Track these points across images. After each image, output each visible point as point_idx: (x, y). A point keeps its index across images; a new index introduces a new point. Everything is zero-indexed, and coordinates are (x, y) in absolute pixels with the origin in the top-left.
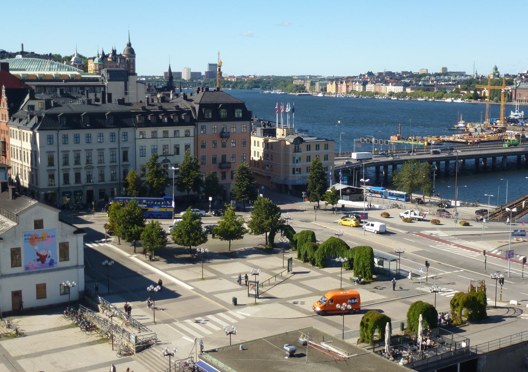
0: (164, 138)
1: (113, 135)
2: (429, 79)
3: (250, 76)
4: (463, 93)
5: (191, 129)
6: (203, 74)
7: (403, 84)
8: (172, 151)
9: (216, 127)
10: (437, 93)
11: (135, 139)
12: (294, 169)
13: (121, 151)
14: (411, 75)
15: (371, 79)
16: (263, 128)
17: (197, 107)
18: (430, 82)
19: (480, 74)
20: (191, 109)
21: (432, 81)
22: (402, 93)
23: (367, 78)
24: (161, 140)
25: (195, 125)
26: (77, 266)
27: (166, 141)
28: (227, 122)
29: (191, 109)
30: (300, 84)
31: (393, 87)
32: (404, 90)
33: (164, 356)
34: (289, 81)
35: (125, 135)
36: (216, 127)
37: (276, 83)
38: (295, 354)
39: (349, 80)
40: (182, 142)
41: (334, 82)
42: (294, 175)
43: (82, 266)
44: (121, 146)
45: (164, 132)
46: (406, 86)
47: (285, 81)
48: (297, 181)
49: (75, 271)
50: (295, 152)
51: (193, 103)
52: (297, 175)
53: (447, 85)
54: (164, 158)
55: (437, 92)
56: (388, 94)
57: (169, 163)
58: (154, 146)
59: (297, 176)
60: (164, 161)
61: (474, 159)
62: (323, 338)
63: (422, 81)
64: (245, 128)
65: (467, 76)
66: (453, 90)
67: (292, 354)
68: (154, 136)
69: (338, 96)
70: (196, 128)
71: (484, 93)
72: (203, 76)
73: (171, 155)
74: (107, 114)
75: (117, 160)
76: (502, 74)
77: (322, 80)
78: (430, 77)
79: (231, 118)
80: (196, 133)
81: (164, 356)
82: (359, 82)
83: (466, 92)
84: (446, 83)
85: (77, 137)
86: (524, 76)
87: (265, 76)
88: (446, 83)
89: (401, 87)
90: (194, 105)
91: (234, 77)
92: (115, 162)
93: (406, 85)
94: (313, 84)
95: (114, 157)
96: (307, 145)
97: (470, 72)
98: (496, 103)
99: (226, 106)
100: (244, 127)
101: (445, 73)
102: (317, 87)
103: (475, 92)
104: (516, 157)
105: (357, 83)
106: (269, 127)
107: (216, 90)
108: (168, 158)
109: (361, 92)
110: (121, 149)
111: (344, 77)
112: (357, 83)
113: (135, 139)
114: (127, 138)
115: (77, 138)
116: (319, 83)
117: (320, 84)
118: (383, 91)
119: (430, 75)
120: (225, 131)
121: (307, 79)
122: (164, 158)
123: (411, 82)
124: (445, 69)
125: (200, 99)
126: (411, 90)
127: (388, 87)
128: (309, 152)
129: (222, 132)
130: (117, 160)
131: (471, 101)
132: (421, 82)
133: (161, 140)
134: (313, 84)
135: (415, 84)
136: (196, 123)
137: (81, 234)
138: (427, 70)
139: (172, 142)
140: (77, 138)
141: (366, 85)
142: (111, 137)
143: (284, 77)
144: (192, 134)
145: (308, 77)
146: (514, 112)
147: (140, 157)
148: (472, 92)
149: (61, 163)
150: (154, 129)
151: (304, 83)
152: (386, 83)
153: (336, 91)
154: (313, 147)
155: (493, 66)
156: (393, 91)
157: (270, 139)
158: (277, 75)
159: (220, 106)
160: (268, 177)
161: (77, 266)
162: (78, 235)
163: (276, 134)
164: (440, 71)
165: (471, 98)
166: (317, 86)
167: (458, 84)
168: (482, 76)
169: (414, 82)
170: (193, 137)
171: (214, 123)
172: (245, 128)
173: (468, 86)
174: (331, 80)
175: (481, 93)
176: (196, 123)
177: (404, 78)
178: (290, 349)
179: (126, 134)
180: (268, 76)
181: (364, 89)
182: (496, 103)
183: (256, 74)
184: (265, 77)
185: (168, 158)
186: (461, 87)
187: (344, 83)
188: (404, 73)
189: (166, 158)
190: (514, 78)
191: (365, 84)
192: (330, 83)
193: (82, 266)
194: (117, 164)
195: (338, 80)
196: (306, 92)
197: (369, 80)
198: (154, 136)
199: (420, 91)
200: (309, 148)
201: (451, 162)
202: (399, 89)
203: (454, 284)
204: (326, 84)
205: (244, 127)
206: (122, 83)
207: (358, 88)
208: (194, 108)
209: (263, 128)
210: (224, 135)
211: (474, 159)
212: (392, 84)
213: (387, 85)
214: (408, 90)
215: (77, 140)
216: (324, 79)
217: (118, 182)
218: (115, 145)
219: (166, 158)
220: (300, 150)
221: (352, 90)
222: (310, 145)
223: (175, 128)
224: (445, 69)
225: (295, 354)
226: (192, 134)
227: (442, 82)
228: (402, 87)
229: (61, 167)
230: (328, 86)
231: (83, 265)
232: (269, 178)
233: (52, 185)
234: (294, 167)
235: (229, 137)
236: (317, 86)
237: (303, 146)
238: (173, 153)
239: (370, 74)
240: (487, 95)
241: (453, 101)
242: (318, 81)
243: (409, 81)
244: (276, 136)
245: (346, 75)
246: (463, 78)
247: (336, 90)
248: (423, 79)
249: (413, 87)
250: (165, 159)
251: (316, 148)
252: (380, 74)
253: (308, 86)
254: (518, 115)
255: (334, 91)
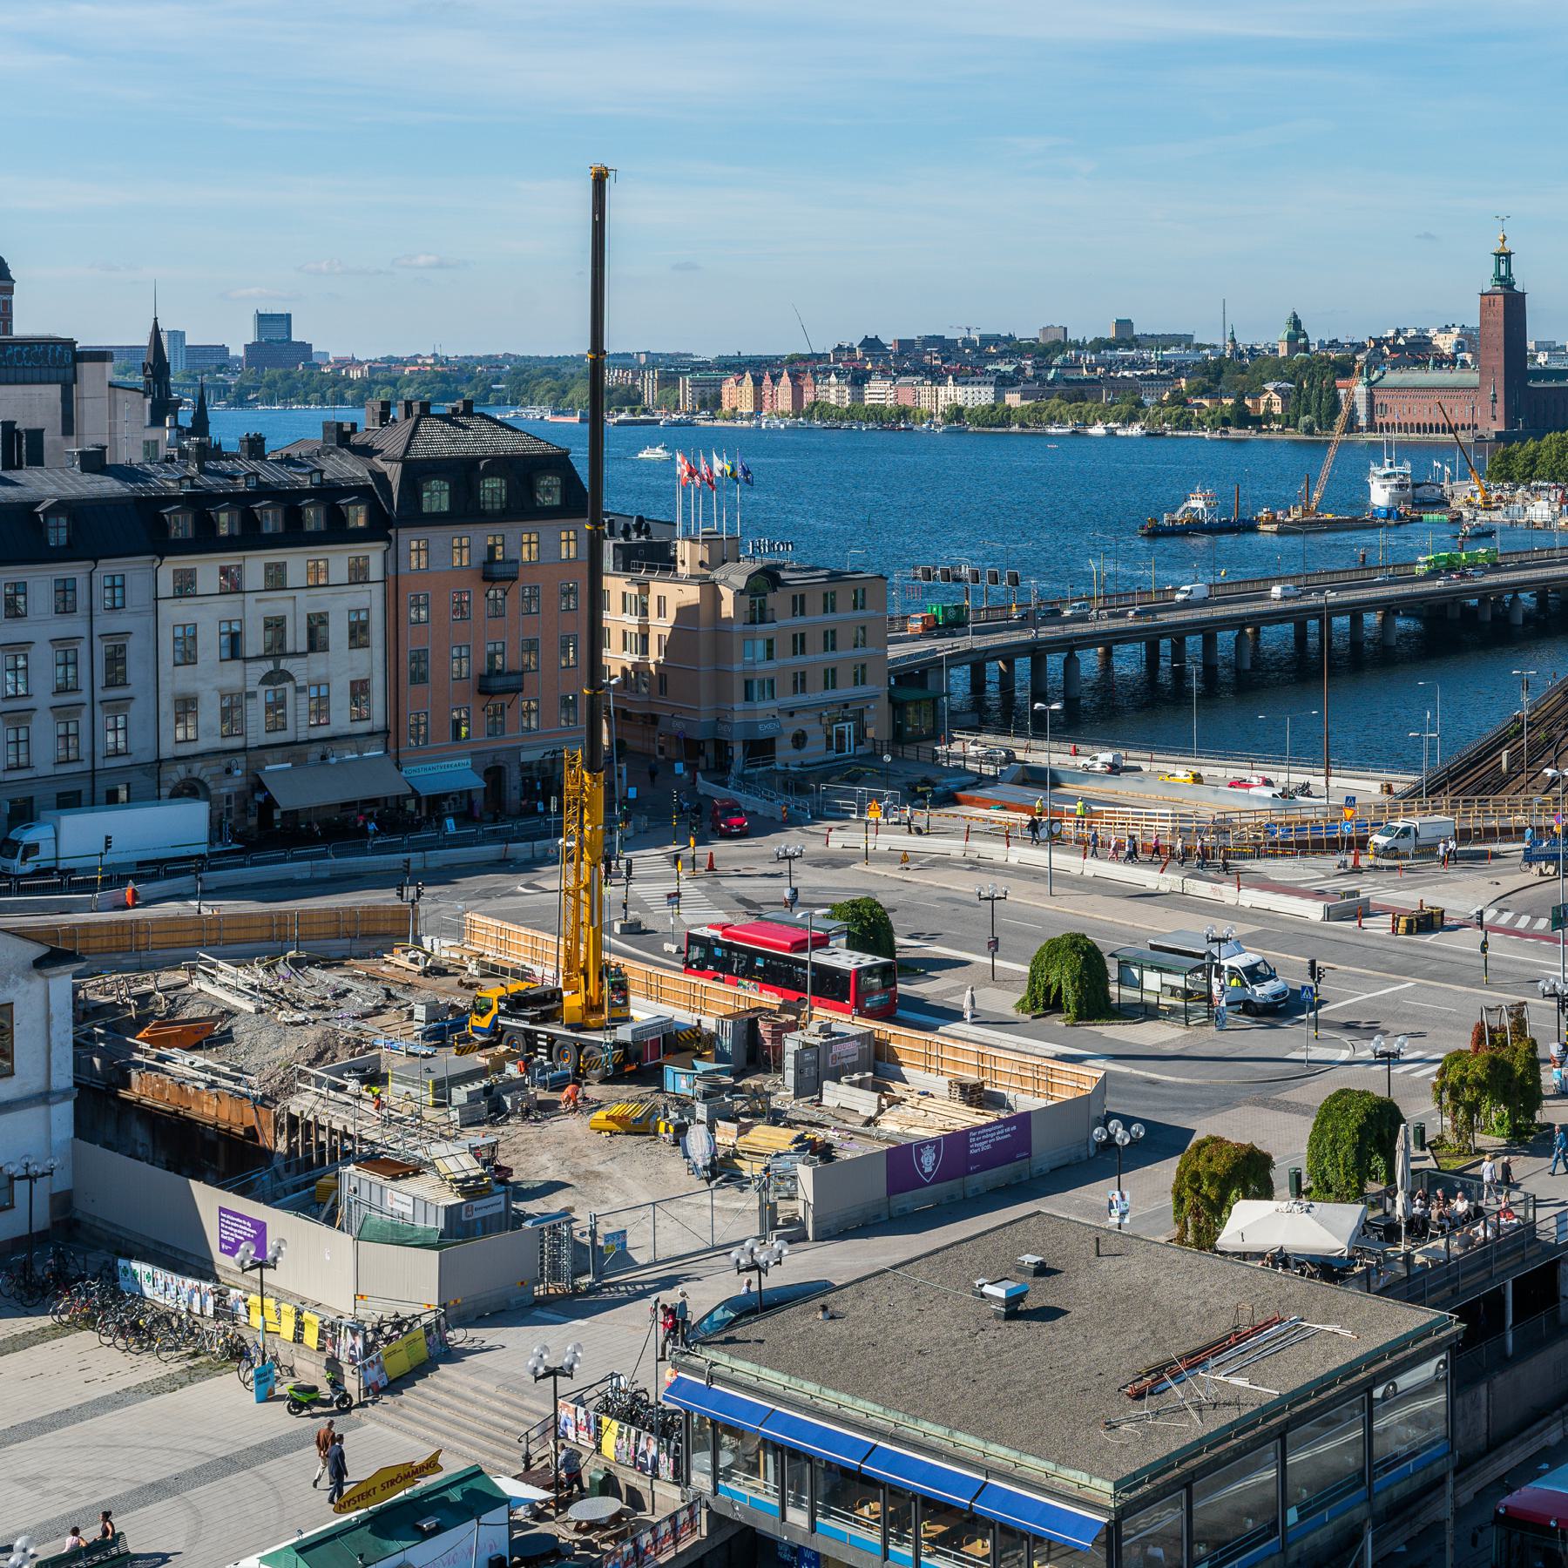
0: (351, 583)
1: (65, 590)
2: (1077, 358)
3: (419, 356)
4: (1200, 406)
5: (374, 554)
6: (237, 351)
7: (993, 379)
8: (296, 637)
9: (465, 542)
10: (1113, 408)
11: (156, 599)
12: (748, 684)
13: (100, 648)
14: (1011, 347)
15: (875, 363)
16: (622, 540)
17: (394, 472)
18: (1085, 372)
19: (1244, 341)
20: (371, 482)
21: (1092, 368)
22: (994, 408)
23: (862, 360)
24: (258, 601)
25: (388, 539)
26: (45, 1097)
27: (278, 604)
28: (471, 527)
29: (371, 482)
30: (622, 385)
31: (960, 390)
32: (999, 397)
33: (537, 1379)
34: (572, 376)
35: (118, 585)
36: (465, 542)
37: (527, 382)
38: (1022, 1307)
39: (802, 367)
40: (339, 608)
41: (748, 375)
42: (749, 705)
43: (64, 1095)
44: (96, 632)
45: (268, 567)
46: (1003, 385)
47: (556, 375)
48: (760, 727)
49: (34, 1114)
50: (753, 622)
51: (377, 460)
52: (760, 705)
53: (1142, 378)
54: (268, 666)
55: (1113, 403)
56: (943, 414)
57: (288, 686)
58: (230, 622)
59: (764, 707)
60: (267, 679)
61: (967, 667)
62: (1095, 1245)
63: (1057, 367)
64: (572, 544)
65: (1200, 347)
66: (1162, 395)
67: (1014, 1310)
68: (276, 579)
69: (763, 426)
70: (391, 553)
71: (1269, 404)
72: (238, 359)
73: (295, 654)
74: (39, 509)
75: (84, 684)
76: (1316, 335)
77: (699, 369)
78: (1079, 352)
79: (522, 508)
80: (391, 571)
81: (537, 1379)
82: (837, 375)
83: (1206, 403)
84: (1139, 373)
85: (65, 590)
86: (1388, 346)
87: (479, 358)
88: (1139, 373)
89: (983, 389)
90: (381, 464)
91: (354, 363)
92: (76, 690)
93: (1004, 382)
94: (668, 380)
95: (71, 671)
96: (794, 597)
97: (1209, 334)
98: (1308, 438)
99: (503, 465)
100: (568, 540)
101: (1126, 335)
102: (685, 391)
103: (1240, 402)
104: (1289, 628)
105: (833, 379)
106: (643, 538)
107: (461, 409)
108: (285, 664)
109: (848, 410)
110: (96, 641)
111: (777, 358)
112: (833, 379)
113: (156, 599)
114: (123, 597)
115: (233, 585)
116: (691, 380)
117: (696, 384)
118: (925, 404)
119: (1077, 346)
120: (499, 557)
121: (643, 368)
122: (268, 666)
123: (1020, 370)
124: (1124, 325)
125: (404, 443)
126: (1023, 398)
127: (942, 390)
128: (800, 620)
129: (491, 559)
130: (84, 684)
131: (1227, 432)
132: (1053, 371)
133: (258, 601)
134: (668, 380)
135: (1034, 377)
136: (391, 532)
137: (63, 968)
138: (1066, 329)
139: (295, 609)
140: (185, 587)
141: (864, 383)
142: (61, 595)
143: (551, 358)
144: (375, 572)
145: (643, 359)
146: (1381, 465)
147: (221, 660)
148: (1228, 402)
149: (100, 680)
150: (229, 559)
151: (634, 379)
152: (937, 377)
153: (755, 409)
154: (814, 602)
155: (1289, 315)
156: (961, 403)
157: (653, 580)
158: (457, 348)
159: (482, 464)
160: (645, 716)
161: (45, 1097)
162: (46, 972)
163: (673, 560)
164: (1110, 333)
165: (1226, 422)
166: (684, 393)
167: (1178, 374)
168: (1252, 350)
169: (1029, 372)
170: (381, 585)
171: (567, 521)
172: (465, 552)
173: (1210, 380)
174: (735, 366)
175: (1257, 405)
176: (391, 532)
177: (993, 358)
178: (1007, 1292)
179: (118, 581)
180: (490, 357)
181: (858, 397)
182: (1308, 438)
183: (437, 347)
184: (480, 361)
185: (285, 664)
186: (1188, 385)
187: (785, 380)
188: (987, 340)
189: (277, 664)
190: (1357, 352)
191: (859, 380)
192: (732, 380)
193: (64, 1095)
194: (84, 697)
195: (760, 369)
196: (645, 411)
197: (869, 367)
198: (233, 585)
199: (1056, 401)
200: (799, 605)
201: (1337, 621)
202: (978, 396)
203: (1421, 1035)
204: (718, 384)
205: (461, 547)
206: (54, 391)
207: (835, 393)
208: (381, 478)
209: (622, 540)
210: (494, 572)
211: (967, 667)
212: (955, 380)
213: (939, 384)
214: (1013, 399)
215: (114, 598)
216: (703, 366)
217: (86, 766)
218: (74, 626)
219: (277, 664)
220: (769, 615)
221: (816, 404)
222: (802, 597)
223: (310, 552)
224: (1124, 325)
225: (1022, 1307)
226: (375, 572)
227: (1125, 368)
228: (992, 389)
229: (100, 695)
230: (725, 389)
231: (69, 1089)
232: (654, 719)
233: (19, 767)
234: (749, 677)
235: (515, 579)
236: (684, 393)
237: (777, 601)
238: (303, 647)
239: (871, 344)
240: (1277, 410)
241: (1111, 433)
242: (688, 373)
243: (1010, 368)
244: (675, 569)
245: (787, 350)
246: (1191, 356)
247: (755, 404)
248: (1058, 361)
249: (1029, 387)
250: (272, 668)
251: (794, 610)
252: (905, 345)
253: (649, 388)
254: (1394, 475)
255: (747, 408)
